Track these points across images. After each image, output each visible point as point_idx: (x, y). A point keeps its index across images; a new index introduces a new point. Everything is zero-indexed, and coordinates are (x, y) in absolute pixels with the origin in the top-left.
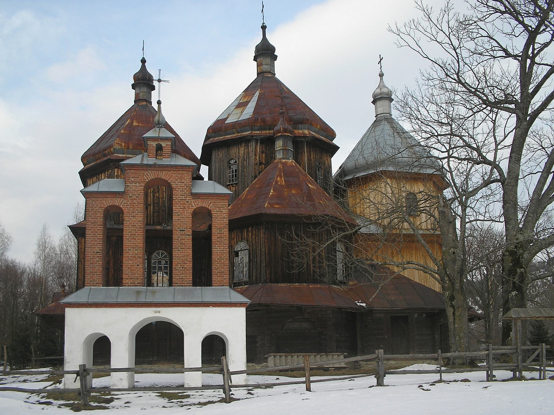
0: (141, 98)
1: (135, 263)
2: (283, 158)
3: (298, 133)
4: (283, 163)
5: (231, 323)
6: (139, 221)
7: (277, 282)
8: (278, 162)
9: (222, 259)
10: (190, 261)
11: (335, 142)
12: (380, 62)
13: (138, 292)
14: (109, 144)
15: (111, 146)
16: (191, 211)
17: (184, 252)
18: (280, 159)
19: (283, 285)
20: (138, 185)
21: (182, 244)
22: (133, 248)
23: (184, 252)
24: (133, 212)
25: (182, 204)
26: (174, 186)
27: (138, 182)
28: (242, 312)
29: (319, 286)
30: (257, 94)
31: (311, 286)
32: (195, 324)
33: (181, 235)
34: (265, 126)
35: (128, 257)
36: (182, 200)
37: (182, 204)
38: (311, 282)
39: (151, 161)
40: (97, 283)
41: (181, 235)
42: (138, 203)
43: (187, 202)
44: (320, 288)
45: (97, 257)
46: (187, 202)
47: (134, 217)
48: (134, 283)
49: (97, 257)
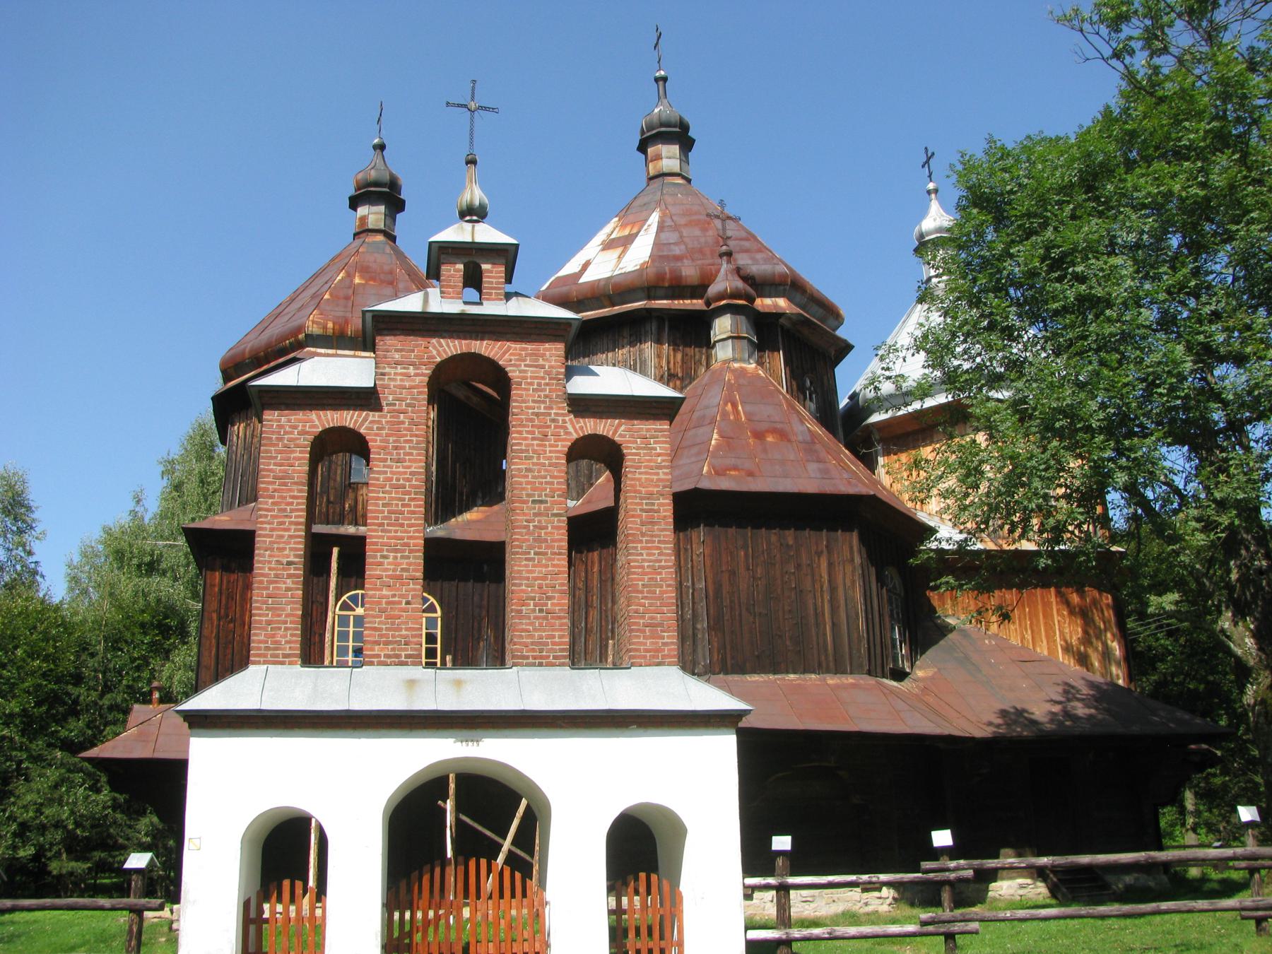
0: (370, 227)
1: (401, 596)
2: (734, 360)
3: (763, 305)
4: (734, 371)
5: (700, 785)
6: (412, 473)
7: (742, 670)
8: (722, 370)
9: (656, 586)
10: (561, 592)
11: (841, 333)
12: (927, 162)
13: (411, 683)
14: (295, 323)
15: (300, 329)
16: (563, 446)
17: (547, 566)
18: (726, 362)
19: (756, 678)
20: (411, 370)
21: (539, 540)
22: (396, 551)
23: (547, 566)
24: (396, 448)
25: (539, 427)
26: (513, 373)
27: (413, 364)
28: (723, 749)
29: (851, 681)
30: (654, 218)
31: (830, 682)
32: (580, 788)
33: (539, 514)
34: (678, 289)
35: (380, 577)
36: (537, 415)
37: (539, 427)
38: (828, 671)
39: (453, 307)
40: (285, 656)
41: (535, 515)
42: (412, 423)
43: (553, 421)
44: (854, 686)
45: (290, 576)
46: (553, 421)
47: (398, 461)
48: (398, 656)
49: (290, 576)
